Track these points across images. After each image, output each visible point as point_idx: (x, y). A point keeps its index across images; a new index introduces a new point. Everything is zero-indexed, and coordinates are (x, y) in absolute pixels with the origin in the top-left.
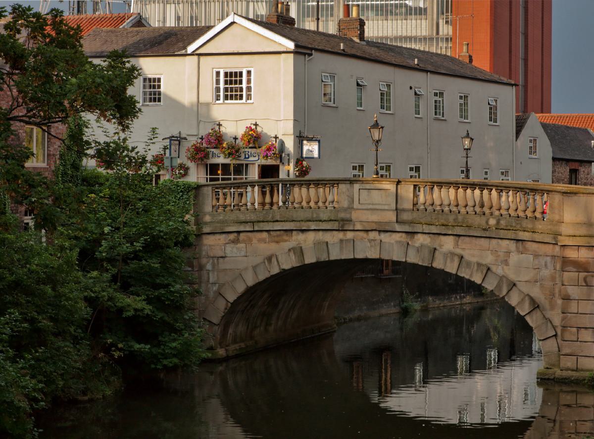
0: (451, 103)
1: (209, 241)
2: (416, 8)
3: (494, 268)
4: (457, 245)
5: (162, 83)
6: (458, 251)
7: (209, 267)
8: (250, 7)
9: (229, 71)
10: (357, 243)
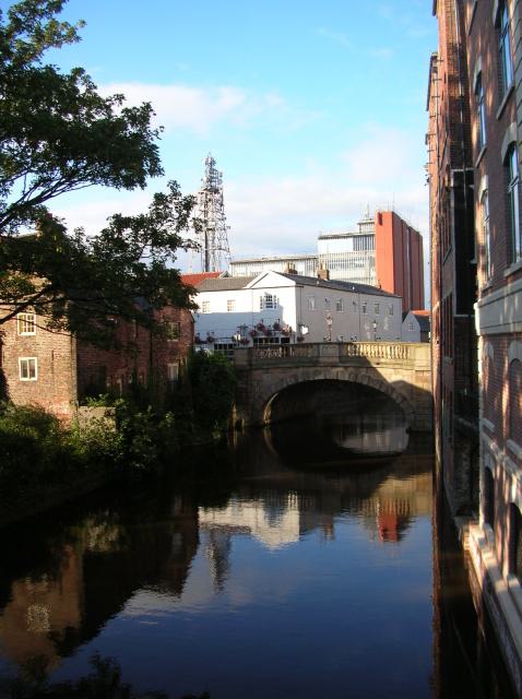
1: (256, 374)
8: (441, 260)
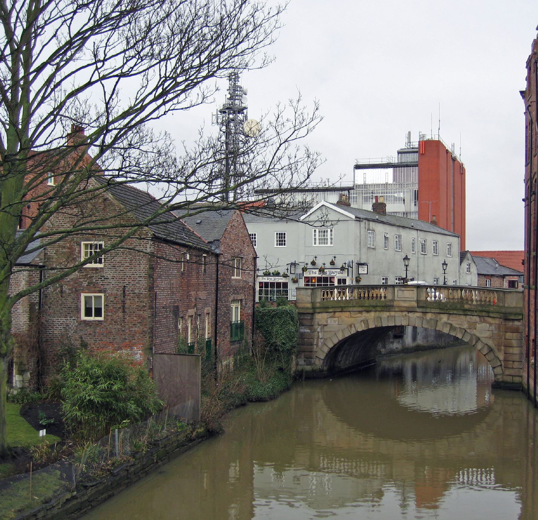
0: (430, 246)
1: (320, 318)
2: (399, 198)
3: (468, 331)
4: (448, 319)
5: (256, 236)
6: (450, 322)
7: (319, 330)
9: (279, 232)
10: (397, 318)
